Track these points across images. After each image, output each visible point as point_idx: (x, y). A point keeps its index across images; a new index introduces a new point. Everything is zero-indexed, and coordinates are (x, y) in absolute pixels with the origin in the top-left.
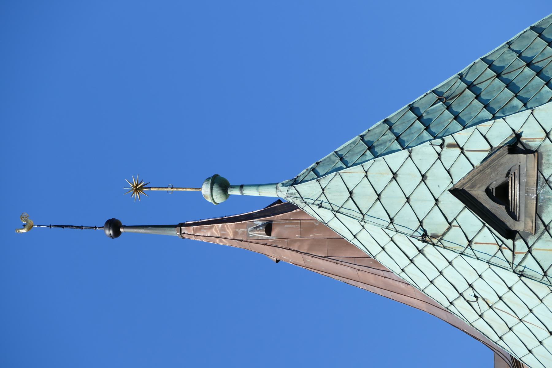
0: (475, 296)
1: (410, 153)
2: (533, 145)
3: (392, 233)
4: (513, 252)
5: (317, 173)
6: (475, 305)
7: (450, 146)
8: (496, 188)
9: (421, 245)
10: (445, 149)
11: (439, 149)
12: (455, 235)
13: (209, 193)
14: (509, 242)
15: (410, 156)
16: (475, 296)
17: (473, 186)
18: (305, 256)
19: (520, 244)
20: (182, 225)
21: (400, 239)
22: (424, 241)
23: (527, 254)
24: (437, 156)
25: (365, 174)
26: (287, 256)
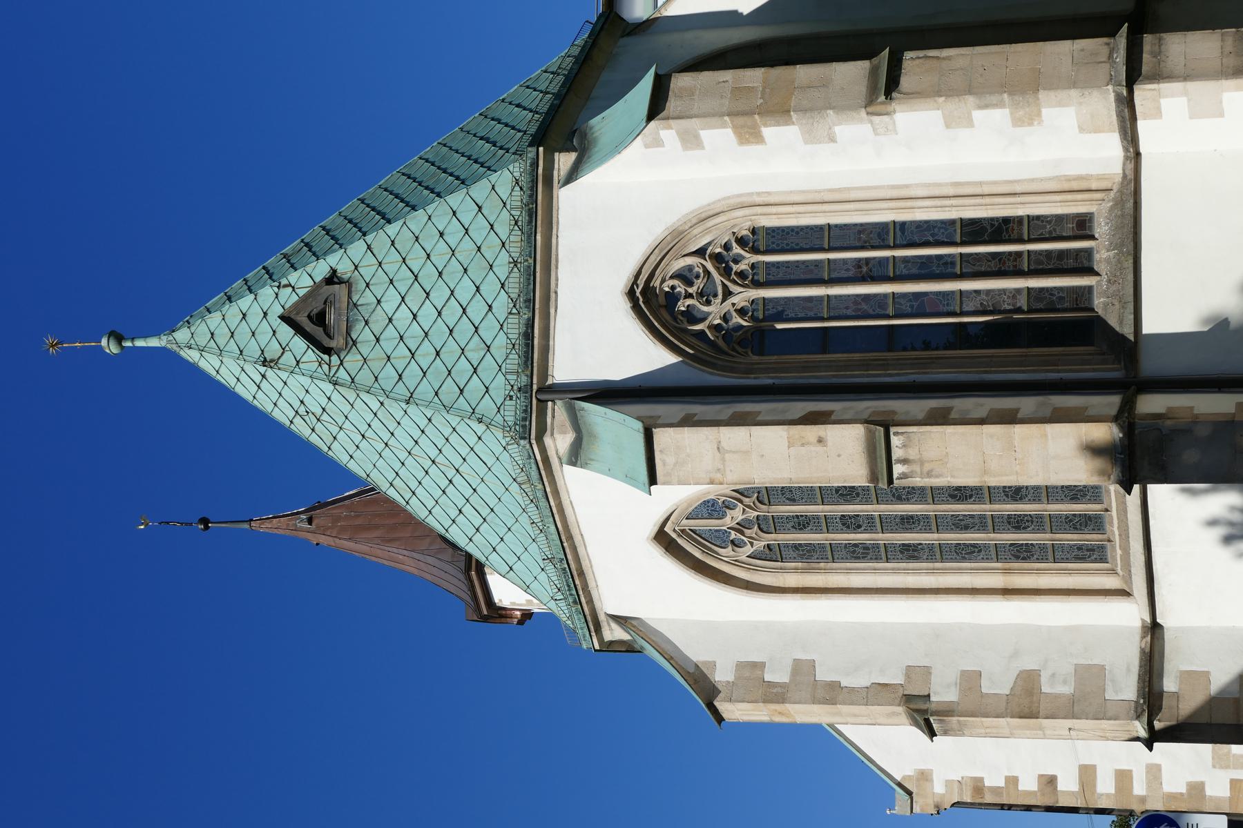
0: (307, 412)
1: (256, 295)
2: (346, 277)
3: (241, 363)
4: (329, 366)
5: (189, 323)
6: (306, 418)
7: (285, 286)
8: (317, 314)
9: (262, 369)
10: (281, 289)
11: (276, 289)
12: (288, 359)
13: (106, 344)
14: (326, 357)
15: (255, 299)
16: (307, 412)
17: (297, 314)
18: (335, 539)
19: (335, 359)
20: (252, 520)
21: (248, 367)
22: (264, 366)
23: (339, 366)
24: (275, 296)
25: (222, 317)
26: (324, 540)
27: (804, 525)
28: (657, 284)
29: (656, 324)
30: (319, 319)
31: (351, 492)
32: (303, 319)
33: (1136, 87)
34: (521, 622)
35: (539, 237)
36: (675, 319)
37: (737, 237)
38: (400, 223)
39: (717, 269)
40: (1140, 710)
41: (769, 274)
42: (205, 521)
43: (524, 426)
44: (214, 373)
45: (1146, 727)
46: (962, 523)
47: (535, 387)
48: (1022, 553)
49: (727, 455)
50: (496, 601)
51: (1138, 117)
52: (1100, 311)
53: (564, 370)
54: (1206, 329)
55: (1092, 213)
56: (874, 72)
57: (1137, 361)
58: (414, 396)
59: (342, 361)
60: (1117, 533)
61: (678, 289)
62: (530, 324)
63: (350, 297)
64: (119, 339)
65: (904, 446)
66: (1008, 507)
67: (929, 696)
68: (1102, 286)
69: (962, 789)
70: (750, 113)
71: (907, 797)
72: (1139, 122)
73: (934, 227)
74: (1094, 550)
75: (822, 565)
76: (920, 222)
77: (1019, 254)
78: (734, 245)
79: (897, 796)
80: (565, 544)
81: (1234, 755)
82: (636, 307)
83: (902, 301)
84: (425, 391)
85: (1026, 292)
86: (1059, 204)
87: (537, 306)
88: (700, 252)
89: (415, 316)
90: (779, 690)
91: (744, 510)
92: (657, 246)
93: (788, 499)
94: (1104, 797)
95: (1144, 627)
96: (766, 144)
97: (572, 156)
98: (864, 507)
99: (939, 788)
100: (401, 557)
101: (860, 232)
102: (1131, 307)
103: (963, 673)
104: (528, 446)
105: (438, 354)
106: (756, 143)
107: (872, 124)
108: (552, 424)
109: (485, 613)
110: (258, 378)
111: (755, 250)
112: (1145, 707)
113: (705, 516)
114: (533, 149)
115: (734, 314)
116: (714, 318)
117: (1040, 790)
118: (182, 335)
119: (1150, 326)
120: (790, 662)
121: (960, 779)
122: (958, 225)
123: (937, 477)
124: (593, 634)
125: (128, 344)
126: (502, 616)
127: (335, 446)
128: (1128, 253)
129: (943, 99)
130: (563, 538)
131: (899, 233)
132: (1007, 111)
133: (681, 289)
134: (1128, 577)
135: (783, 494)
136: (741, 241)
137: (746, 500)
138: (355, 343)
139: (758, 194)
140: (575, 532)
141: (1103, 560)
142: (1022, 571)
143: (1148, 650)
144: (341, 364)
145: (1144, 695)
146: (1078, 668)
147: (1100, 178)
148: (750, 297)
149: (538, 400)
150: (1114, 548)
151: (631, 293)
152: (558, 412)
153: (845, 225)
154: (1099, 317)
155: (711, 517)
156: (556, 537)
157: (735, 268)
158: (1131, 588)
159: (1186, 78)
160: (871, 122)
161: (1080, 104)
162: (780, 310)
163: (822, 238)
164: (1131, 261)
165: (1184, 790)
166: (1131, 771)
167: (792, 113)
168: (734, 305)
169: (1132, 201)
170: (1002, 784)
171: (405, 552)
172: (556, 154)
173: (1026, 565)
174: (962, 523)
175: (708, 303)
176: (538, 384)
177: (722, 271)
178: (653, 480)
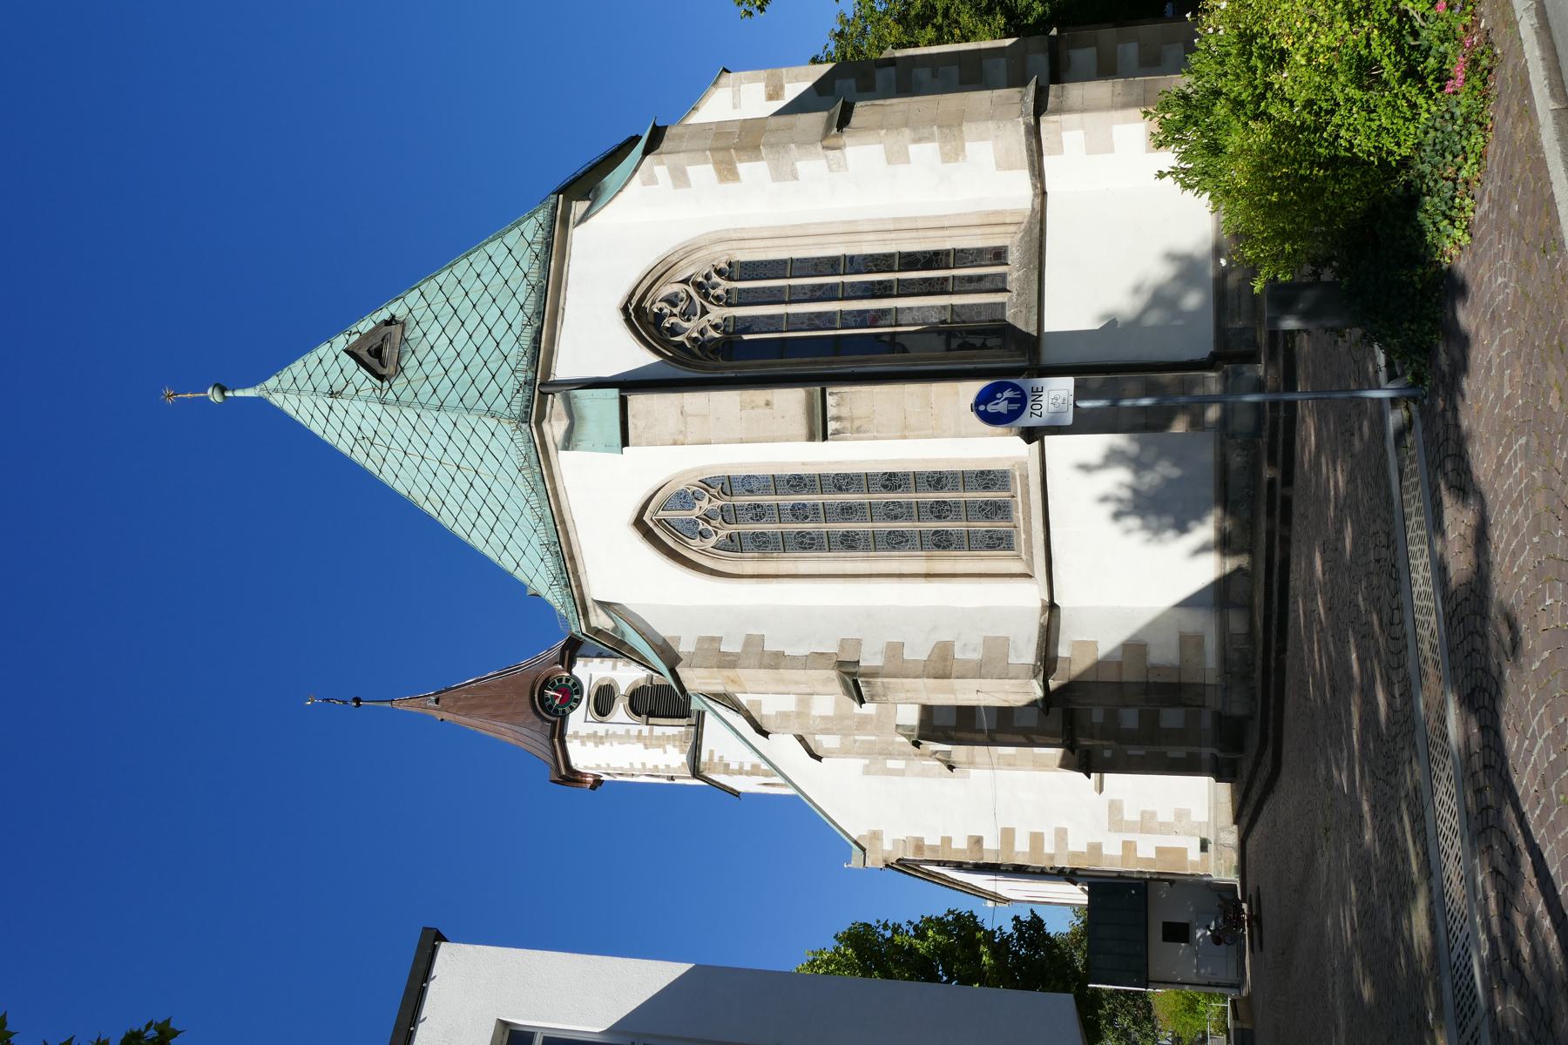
7: (355, 333)
9: (329, 401)
12: (351, 390)
14: (378, 383)
17: (359, 349)
19: (386, 384)
26: (446, 716)
27: (760, 516)
28: (648, 305)
29: (644, 333)
30: (377, 353)
31: (471, 680)
32: (363, 353)
33: (1043, 119)
34: (593, 787)
35: (552, 263)
36: (660, 333)
37: (716, 269)
38: (448, 271)
39: (698, 293)
40: (1037, 671)
41: (740, 298)
42: (357, 700)
43: (526, 413)
44: (293, 413)
45: (1041, 683)
46: (893, 513)
47: (538, 383)
48: (942, 542)
49: (689, 419)
50: (573, 764)
51: (1044, 152)
52: (1010, 320)
53: (563, 369)
54: (1097, 327)
55: (1007, 246)
56: (830, 118)
57: (1039, 353)
58: (444, 405)
59: (391, 385)
60: (1021, 518)
61: (665, 311)
62: (539, 331)
63: (403, 334)
64: (223, 390)
65: (838, 405)
66: (931, 495)
67: (858, 661)
68: (1012, 300)
69: (906, 847)
70: (727, 149)
71: (861, 853)
72: (1044, 157)
73: (877, 259)
74: (1002, 539)
75: (775, 555)
76: (866, 255)
77: (946, 279)
78: (714, 274)
79: (853, 853)
80: (558, 527)
81: (1126, 821)
82: (628, 320)
83: (848, 317)
84: (453, 399)
85: (950, 307)
86: (979, 237)
87: (546, 317)
88: (685, 281)
89: (451, 342)
90: (732, 658)
91: (710, 500)
92: (649, 272)
93: (747, 490)
94: (1020, 855)
95: (1043, 607)
96: (741, 182)
97: (587, 203)
98: (810, 497)
99: (887, 846)
100: (503, 729)
101: (816, 265)
102: (1035, 310)
103: (889, 643)
104: (528, 430)
105: (466, 368)
106: (733, 180)
107: (827, 159)
108: (551, 413)
109: (564, 773)
110: (326, 411)
111: (730, 279)
112: (1042, 668)
113: (678, 508)
114: (555, 196)
115: (709, 328)
116: (692, 331)
117: (970, 848)
118: (272, 383)
119: (1050, 326)
120: (743, 637)
121: (905, 839)
122: (897, 257)
123: (864, 432)
124: (581, 617)
125: (229, 394)
126: (578, 781)
128: (1034, 268)
129: (883, 132)
130: (557, 521)
131: (848, 264)
132: (936, 145)
134: (1030, 563)
135: (743, 486)
136: (719, 272)
137: (712, 491)
138: (402, 369)
139: (735, 230)
140: (567, 517)
141: (1010, 548)
142: (942, 558)
143: (1046, 623)
144: (390, 387)
145: (1041, 658)
146: (986, 639)
147: (1013, 213)
148: (723, 315)
149: (540, 392)
150: (1019, 533)
151: (625, 309)
152: (556, 404)
153: (805, 259)
154: (1009, 324)
155: (683, 508)
156: (551, 520)
157: (712, 292)
158: (1033, 570)
159: (1083, 110)
160: (826, 157)
161: (997, 137)
162: (749, 325)
163: (785, 269)
164: (1036, 274)
165: (1085, 849)
166: (1043, 834)
167: (761, 147)
168: (709, 321)
169: (1038, 227)
170: (939, 843)
171: (507, 725)
172: (574, 203)
173: (945, 553)
174: (893, 513)
175: (689, 320)
176: (541, 379)
177: (702, 295)
178: (625, 442)
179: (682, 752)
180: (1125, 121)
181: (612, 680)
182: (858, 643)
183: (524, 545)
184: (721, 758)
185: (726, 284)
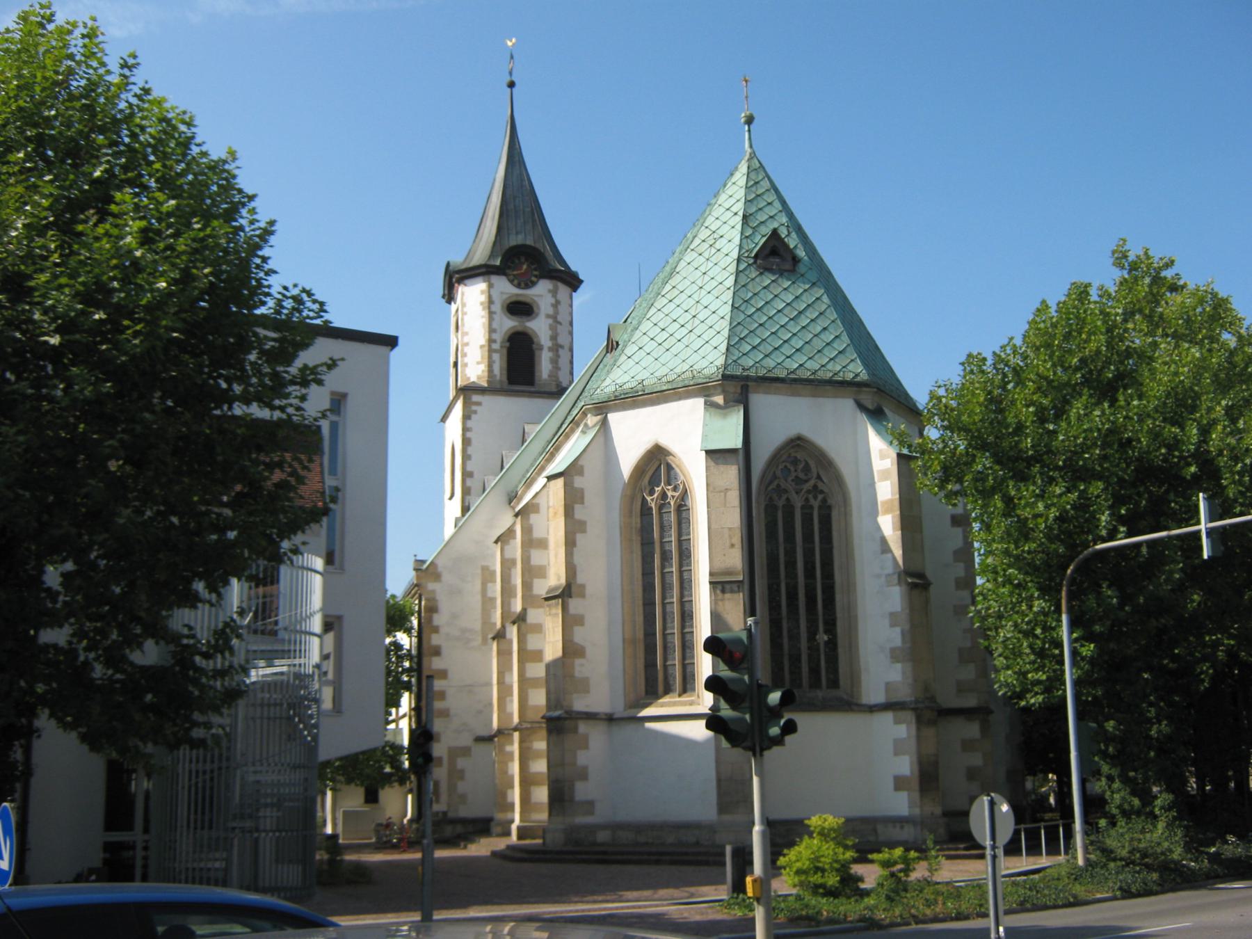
33: (563, 581)
63: (786, 271)
88: (819, 477)
111: (820, 508)
127: (695, 255)
133: (801, 466)
160: (894, 573)
179: (479, 378)
180: (911, 763)
181: (537, 315)
182: (583, 595)
183: (643, 364)
184: (475, 412)
185: (816, 504)
